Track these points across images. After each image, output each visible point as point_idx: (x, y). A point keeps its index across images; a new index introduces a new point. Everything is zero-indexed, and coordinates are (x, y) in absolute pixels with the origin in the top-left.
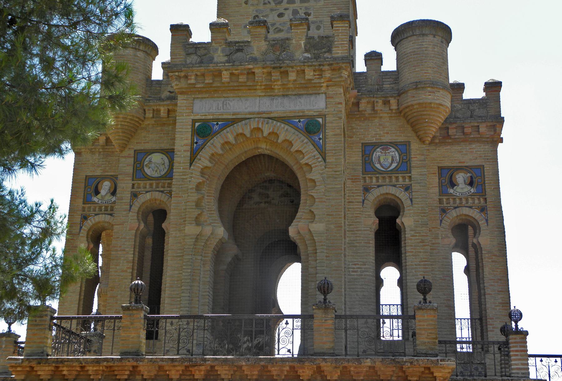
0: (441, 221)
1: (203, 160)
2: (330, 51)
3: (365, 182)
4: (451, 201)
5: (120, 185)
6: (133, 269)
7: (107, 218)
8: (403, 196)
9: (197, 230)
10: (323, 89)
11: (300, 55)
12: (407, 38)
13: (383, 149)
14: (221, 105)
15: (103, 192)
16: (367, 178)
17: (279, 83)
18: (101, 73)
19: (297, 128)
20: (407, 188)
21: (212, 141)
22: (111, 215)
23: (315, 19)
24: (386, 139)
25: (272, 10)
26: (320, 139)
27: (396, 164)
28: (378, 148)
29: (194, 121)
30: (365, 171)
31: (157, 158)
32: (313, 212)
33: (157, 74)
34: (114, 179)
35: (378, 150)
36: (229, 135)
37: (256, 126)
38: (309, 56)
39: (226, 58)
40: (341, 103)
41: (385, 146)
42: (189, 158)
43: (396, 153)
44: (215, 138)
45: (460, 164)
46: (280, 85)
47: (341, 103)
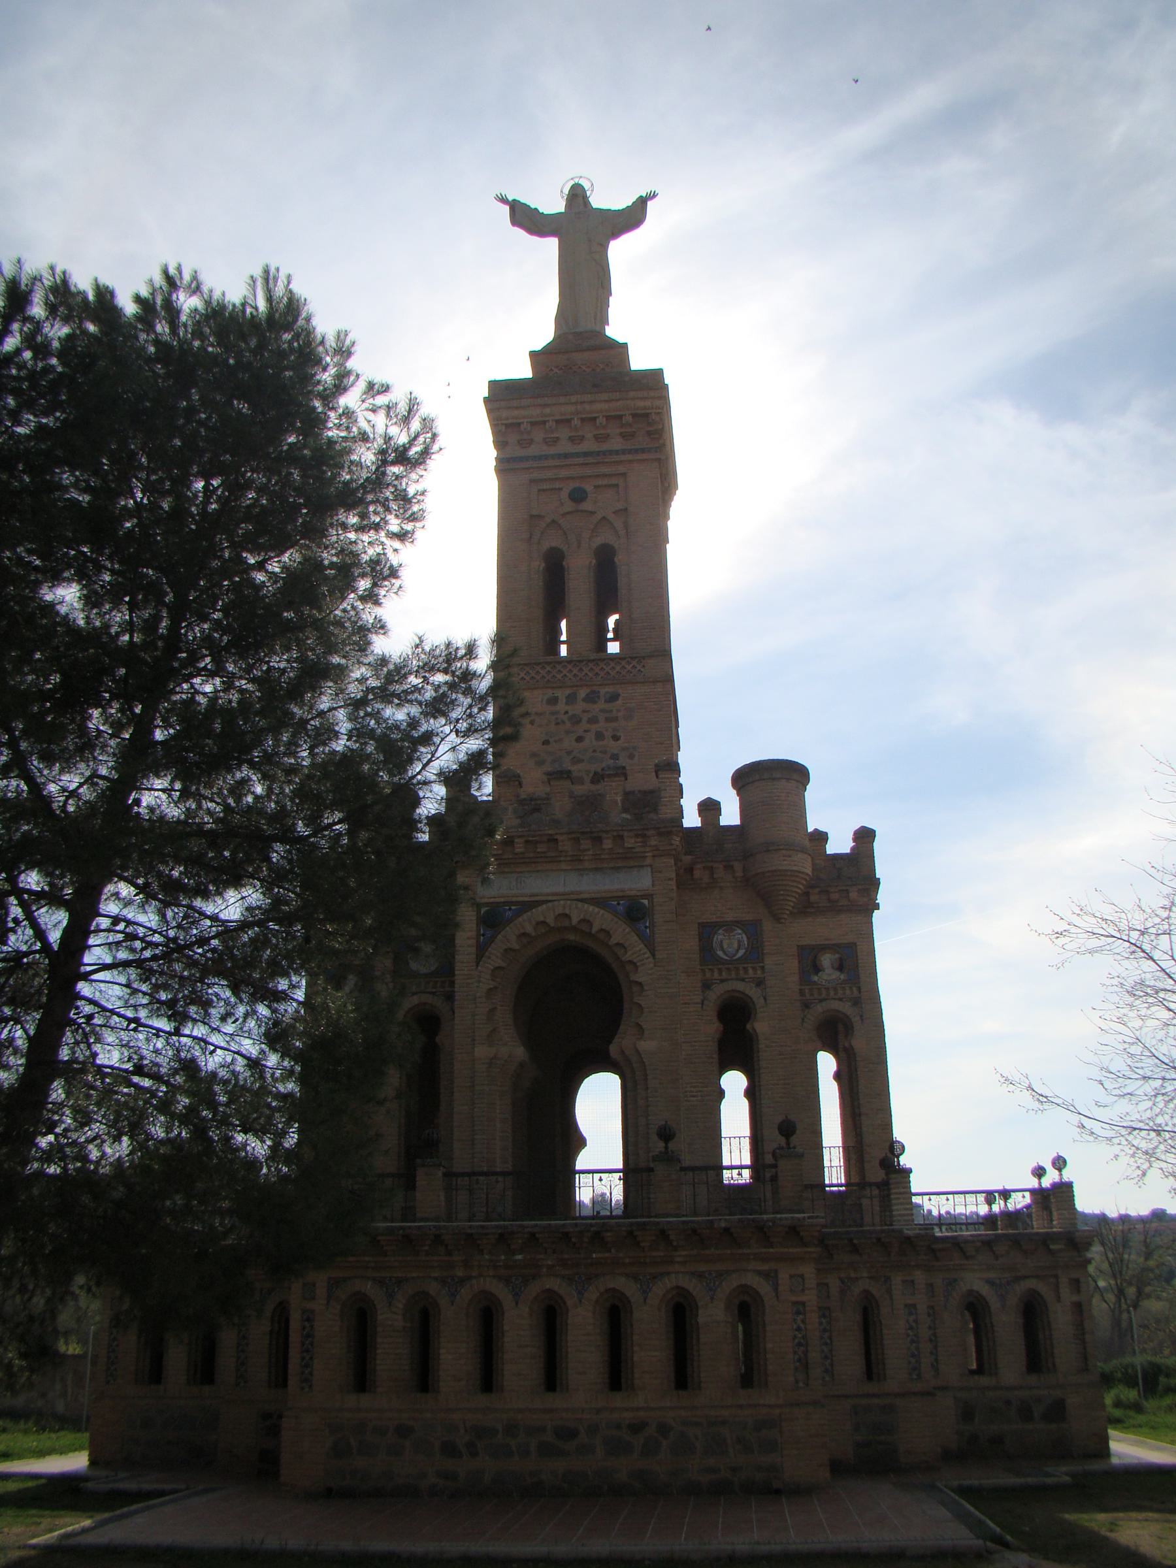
0: (803, 1019)
1: (495, 958)
2: (655, 811)
3: (705, 975)
8: (752, 992)
10: (648, 861)
11: (618, 817)
12: (753, 782)
16: (707, 970)
17: (591, 852)
20: (760, 983)
21: (503, 933)
23: (626, 745)
24: (730, 916)
25: (568, 732)
26: (646, 927)
27: (744, 951)
28: (719, 929)
32: (639, 1025)
35: (720, 931)
36: (526, 923)
37: (561, 912)
38: (628, 817)
39: (518, 821)
40: (670, 879)
41: (729, 926)
42: (474, 956)
43: (744, 936)
44: (508, 928)
45: (827, 942)
46: (592, 855)
47: (670, 879)
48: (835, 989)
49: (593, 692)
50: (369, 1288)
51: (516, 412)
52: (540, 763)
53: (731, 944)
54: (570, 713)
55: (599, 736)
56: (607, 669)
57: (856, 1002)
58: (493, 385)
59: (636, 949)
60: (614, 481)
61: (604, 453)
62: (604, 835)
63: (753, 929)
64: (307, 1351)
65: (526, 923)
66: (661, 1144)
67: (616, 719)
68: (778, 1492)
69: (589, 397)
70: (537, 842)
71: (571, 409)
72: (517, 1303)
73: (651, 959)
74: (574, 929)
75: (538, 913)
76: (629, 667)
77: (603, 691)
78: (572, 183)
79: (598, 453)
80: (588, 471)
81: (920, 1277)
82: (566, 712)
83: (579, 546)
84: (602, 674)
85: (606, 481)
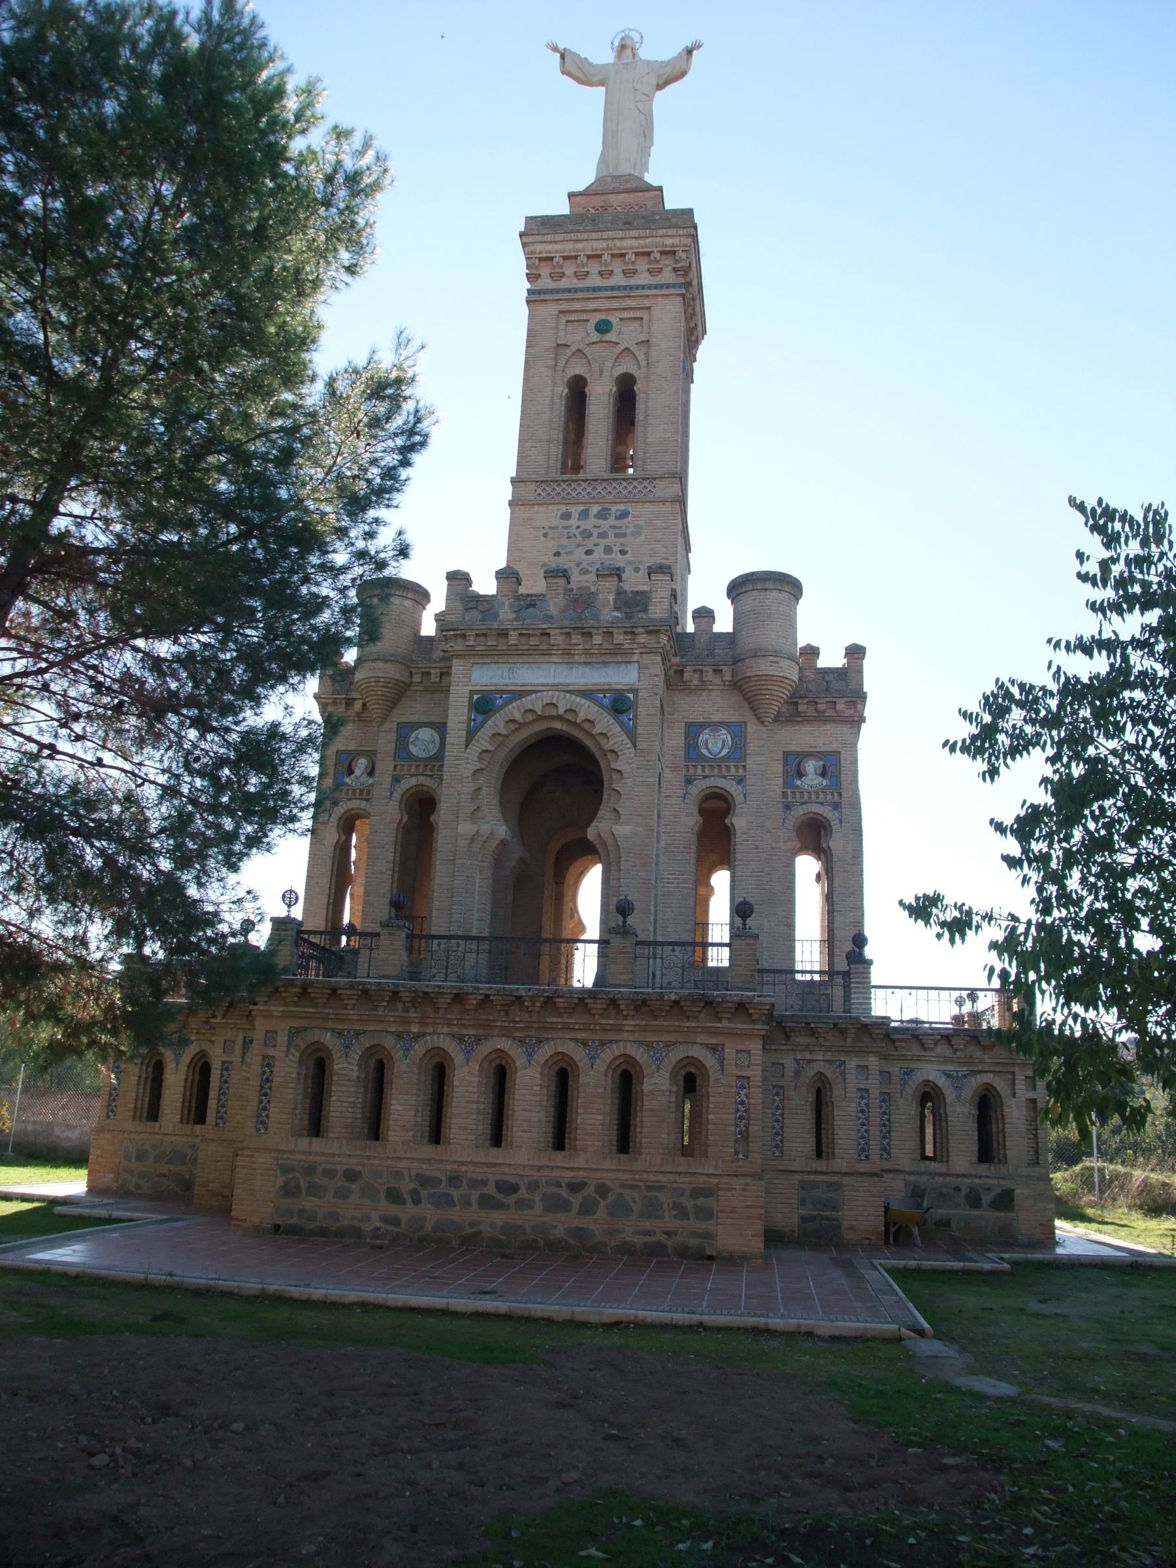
1: (483, 740)
2: (645, 610)
4: (798, 795)
5: (380, 767)
6: (394, 871)
7: (363, 804)
9: (474, 828)
10: (636, 657)
11: (609, 614)
13: (712, 731)
14: (506, 674)
15: (358, 772)
19: (601, 705)
20: (740, 781)
22: (367, 800)
24: (716, 718)
25: (578, 546)
29: (472, 693)
30: (688, 758)
31: (425, 734)
33: (428, 628)
34: (371, 755)
36: (515, 710)
39: (514, 615)
41: (715, 726)
48: (817, 793)
49: (606, 509)
50: (328, 1038)
51: (549, 247)
53: (716, 743)
54: (582, 528)
55: (608, 550)
56: (620, 488)
57: (836, 806)
58: (527, 218)
59: (618, 739)
60: (638, 314)
61: (631, 288)
62: (595, 631)
63: (737, 730)
64: (266, 1095)
65: (515, 710)
66: (621, 918)
67: (625, 535)
68: (711, 1258)
69: (620, 234)
70: (529, 635)
71: (603, 244)
72: (468, 1061)
73: (632, 750)
74: (560, 718)
75: (528, 702)
76: (640, 488)
77: (614, 508)
78: (622, 35)
79: (625, 288)
81: (873, 1061)
83: (601, 375)
84: (614, 492)
85: (631, 314)
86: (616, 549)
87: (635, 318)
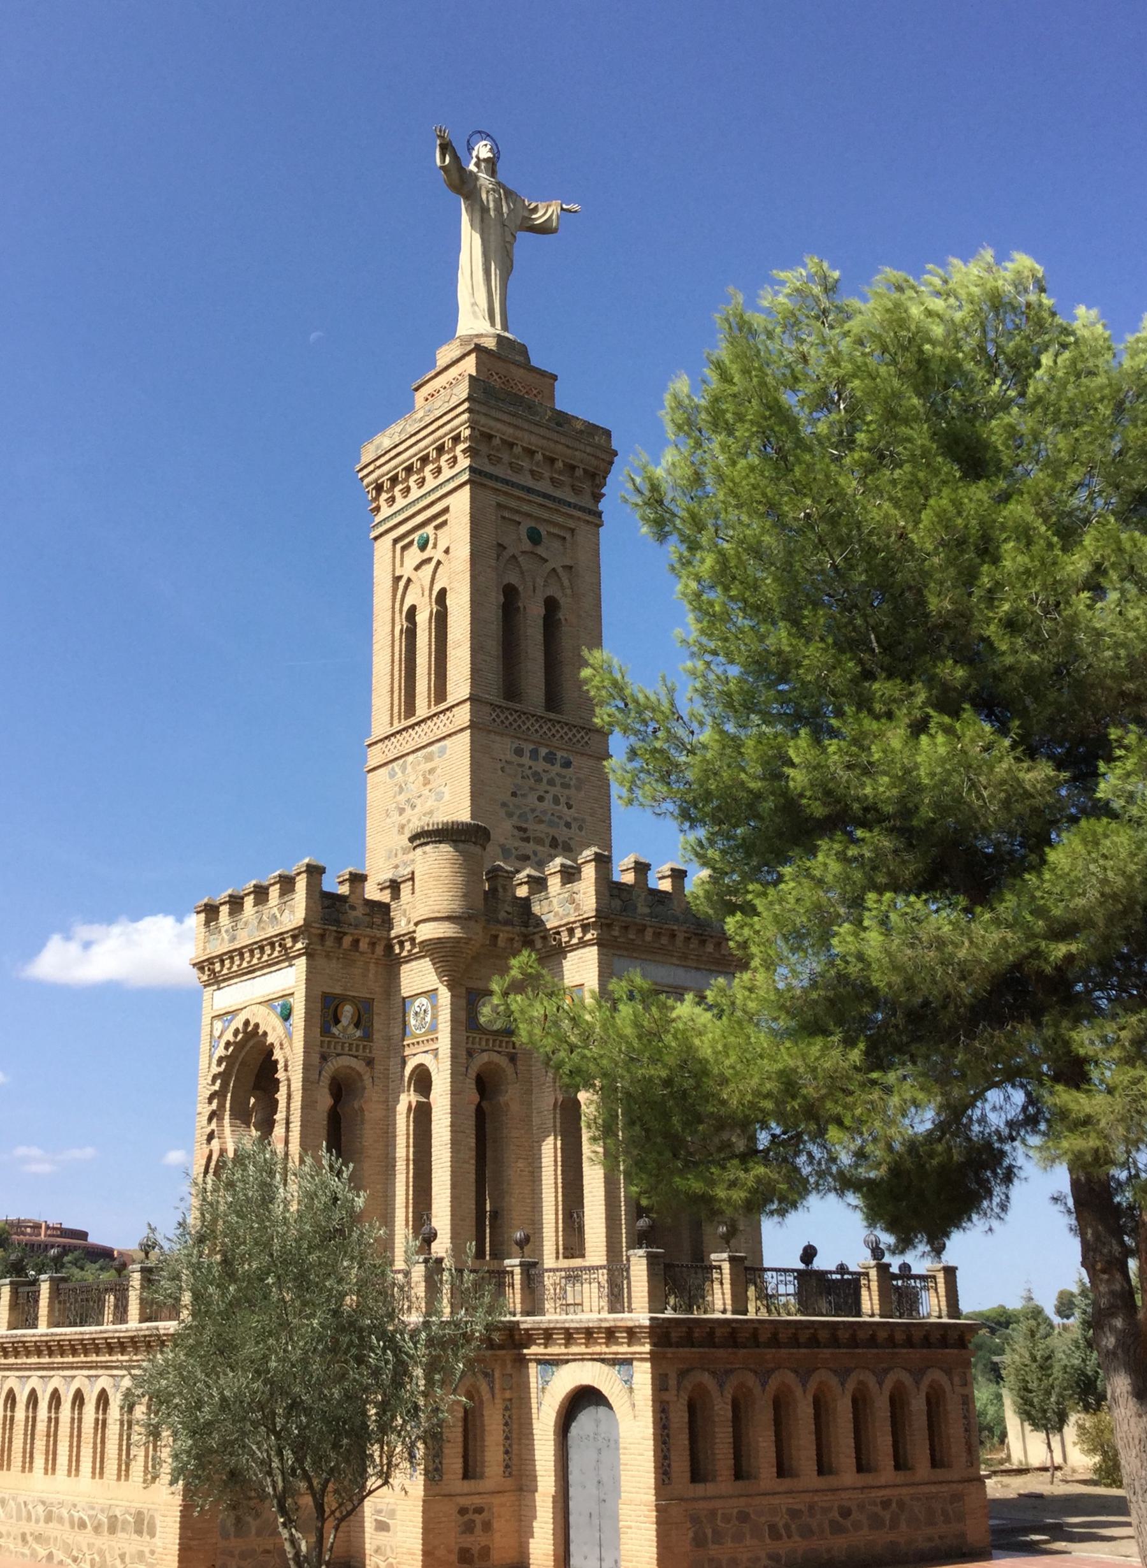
15: (345, 1021)
18: (526, 902)
25: (531, 789)
51: (492, 423)
52: (510, 815)
80: (546, 515)
82: (530, 768)
86: (563, 800)
87: (559, 536)
